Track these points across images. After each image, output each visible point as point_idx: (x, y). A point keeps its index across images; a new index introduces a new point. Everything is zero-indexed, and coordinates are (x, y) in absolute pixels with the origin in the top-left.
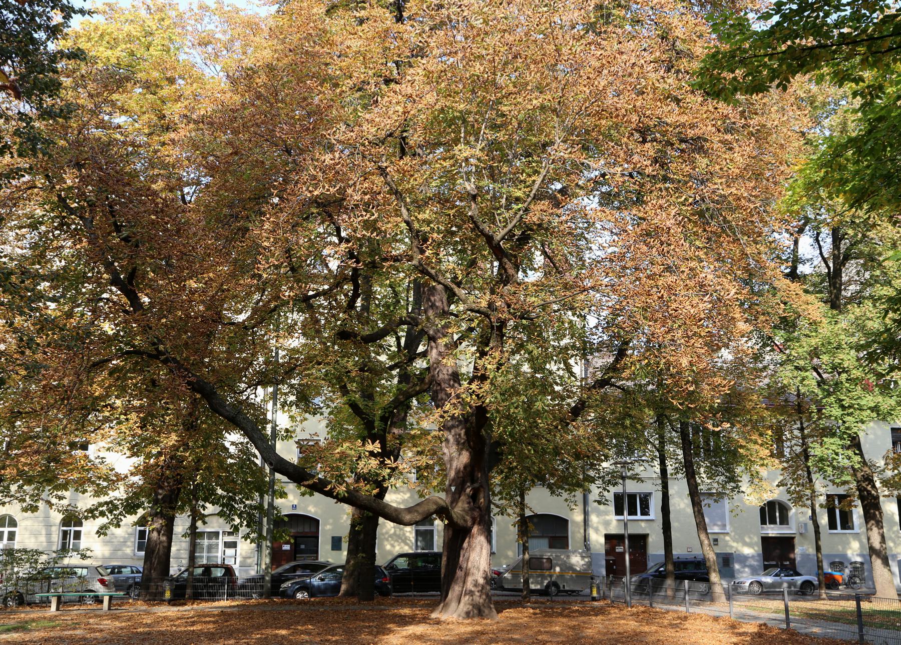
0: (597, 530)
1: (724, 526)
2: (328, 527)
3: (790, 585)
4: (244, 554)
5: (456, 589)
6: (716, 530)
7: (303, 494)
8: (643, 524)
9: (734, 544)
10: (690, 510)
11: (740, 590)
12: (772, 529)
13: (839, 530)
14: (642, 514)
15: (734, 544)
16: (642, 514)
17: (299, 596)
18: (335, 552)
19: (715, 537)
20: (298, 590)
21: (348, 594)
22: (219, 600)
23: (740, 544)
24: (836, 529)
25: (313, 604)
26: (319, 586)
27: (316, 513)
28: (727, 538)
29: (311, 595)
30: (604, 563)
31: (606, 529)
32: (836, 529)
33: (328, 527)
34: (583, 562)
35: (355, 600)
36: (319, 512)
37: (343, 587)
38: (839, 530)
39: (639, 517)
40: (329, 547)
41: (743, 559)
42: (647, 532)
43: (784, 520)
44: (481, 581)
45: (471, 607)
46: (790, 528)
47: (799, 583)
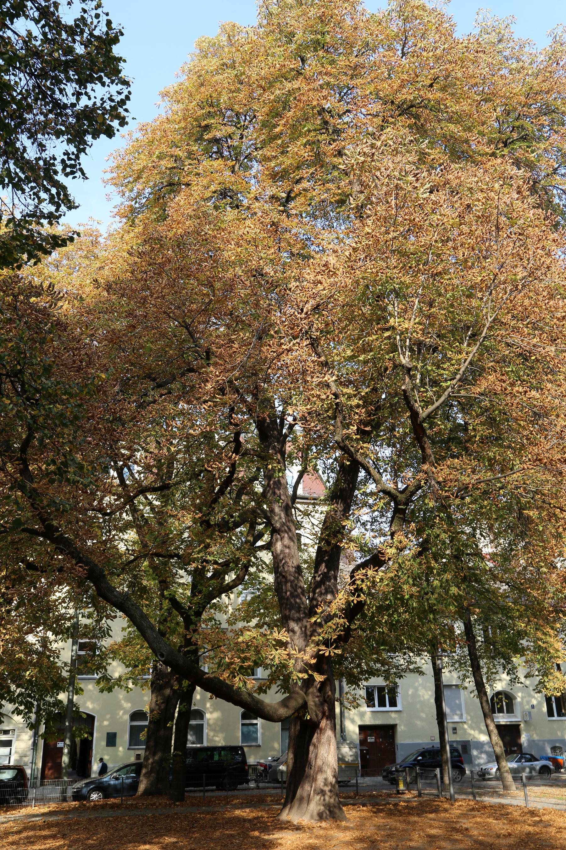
0: (353, 721)
1: (461, 716)
2: (106, 723)
3: (532, 769)
4: (20, 751)
5: (306, 789)
6: (456, 719)
7: (102, 691)
8: (393, 715)
9: (472, 732)
10: (433, 701)
11: (487, 776)
12: (503, 717)
13: (556, 718)
14: (390, 706)
15: (472, 732)
16: (390, 706)
17: (94, 796)
18: (110, 749)
19: (454, 726)
20: (93, 790)
21: (147, 792)
22: (26, 806)
23: (477, 732)
24: (385, 706)
25: (113, 806)
26: (115, 785)
27: (93, 709)
28: (466, 726)
29: (106, 796)
30: (95, 735)
31: (361, 720)
32: (385, 706)
33: (106, 723)
34: (351, 753)
35: (164, 801)
36: (97, 707)
37: (142, 787)
38: (556, 718)
39: (388, 708)
40: (104, 743)
41: (479, 746)
42: (397, 722)
43: (510, 710)
44: (332, 780)
45: (322, 808)
46: (516, 717)
47: (538, 768)
